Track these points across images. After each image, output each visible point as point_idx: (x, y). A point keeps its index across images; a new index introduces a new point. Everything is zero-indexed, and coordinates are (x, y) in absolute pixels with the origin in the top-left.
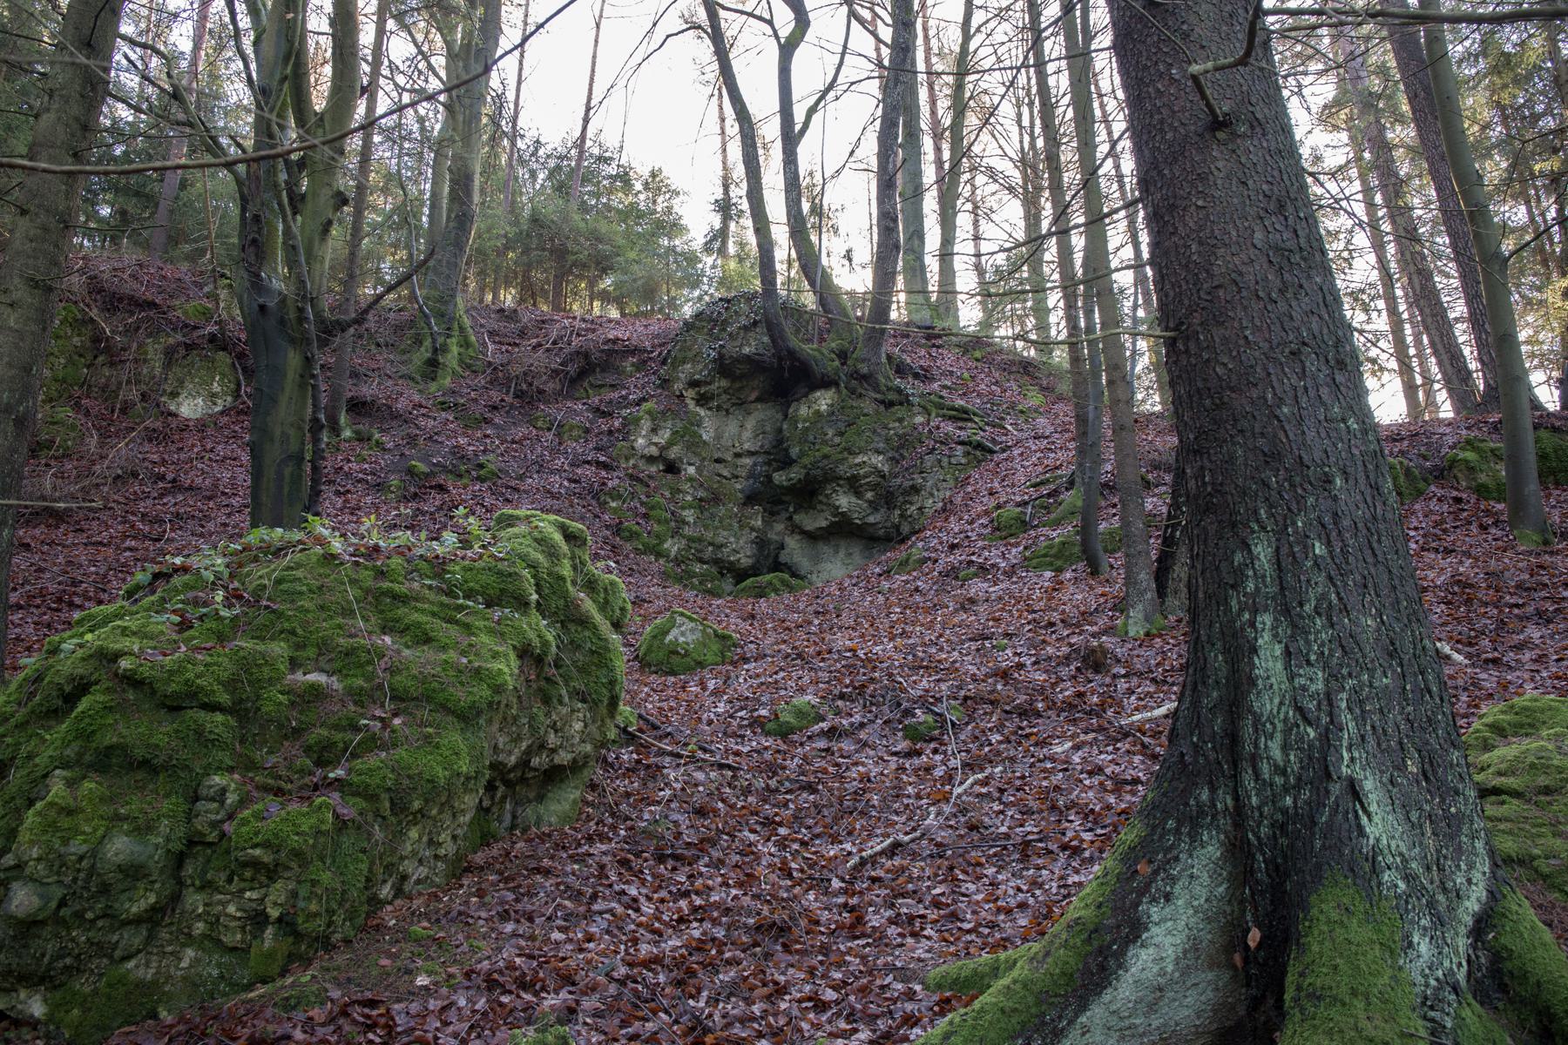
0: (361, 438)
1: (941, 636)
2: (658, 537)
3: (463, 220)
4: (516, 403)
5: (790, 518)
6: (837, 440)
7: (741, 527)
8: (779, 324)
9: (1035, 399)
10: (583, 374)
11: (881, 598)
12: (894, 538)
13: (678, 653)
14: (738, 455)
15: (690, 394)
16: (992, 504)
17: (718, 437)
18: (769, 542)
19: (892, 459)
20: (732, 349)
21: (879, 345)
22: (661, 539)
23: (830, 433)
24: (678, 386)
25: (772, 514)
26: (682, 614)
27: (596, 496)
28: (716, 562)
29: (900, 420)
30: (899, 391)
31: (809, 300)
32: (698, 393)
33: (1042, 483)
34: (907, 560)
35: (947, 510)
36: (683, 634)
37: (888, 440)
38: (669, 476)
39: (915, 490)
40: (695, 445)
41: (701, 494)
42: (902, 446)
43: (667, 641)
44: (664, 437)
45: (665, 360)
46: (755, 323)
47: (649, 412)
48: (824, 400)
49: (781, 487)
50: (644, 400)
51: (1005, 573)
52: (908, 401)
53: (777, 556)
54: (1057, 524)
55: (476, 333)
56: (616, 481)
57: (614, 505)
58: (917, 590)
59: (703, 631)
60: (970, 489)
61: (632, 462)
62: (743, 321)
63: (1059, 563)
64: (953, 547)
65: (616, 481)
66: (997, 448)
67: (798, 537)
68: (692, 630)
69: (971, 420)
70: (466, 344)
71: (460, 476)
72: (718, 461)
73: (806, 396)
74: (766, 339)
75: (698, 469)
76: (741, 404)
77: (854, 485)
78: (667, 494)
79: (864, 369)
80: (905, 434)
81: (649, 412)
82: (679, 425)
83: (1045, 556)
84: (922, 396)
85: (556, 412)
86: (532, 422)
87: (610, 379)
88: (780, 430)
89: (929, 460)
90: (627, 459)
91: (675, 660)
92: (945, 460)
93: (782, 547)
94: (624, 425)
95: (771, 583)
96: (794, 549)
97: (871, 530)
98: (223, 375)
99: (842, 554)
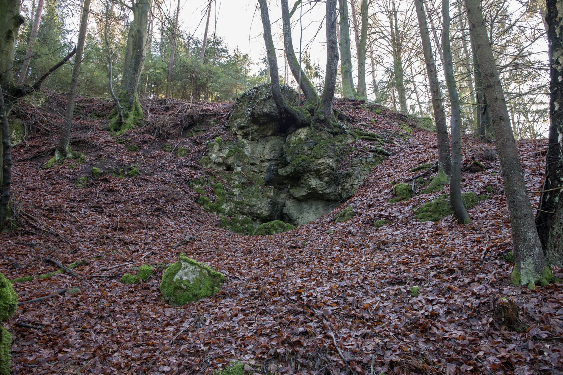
0: (76, 157)
1: (366, 278)
2: (218, 202)
3: (138, 58)
4: (157, 140)
5: (288, 191)
6: (309, 152)
7: (263, 196)
8: (280, 96)
9: (407, 130)
10: (190, 126)
11: (329, 237)
12: (339, 200)
13: (181, 288)
14: (262, 161)
15: (240, 133)
16: (391, 181)
17: (253, 153)
18: (278, 203)
19: (337, 160)
20: (258, 110)
21: (330, 105)
22: (220, 203)
23: (306, 148)
24: (234, 129)
25: (280, 189)
26: (186, 261)
27: (188, 182)
28: (251, 214)
29: (341, 141)
30: (340, 127)
31: (295, 86)
32: (243, 132)
33: (419, 169)
34: (344, 214)
35: (366, 185)
36: (186, 274)
37: (335, 151)
38: (227, 172)
39: (349, 175)
40: (240, 156)
41: (243, 180)
42: (342, 154)
43: (174, 280)
44: (225, 153)
45: (228, 117)
46: (269, 97)
47: (218, 142)
48: (303, 133)
49: (283, 176)
50: (217, 136)
51: (402, 222)
52: (344, 132)
53: (282, 210)
54: (431, 191)
55: (143, 109)
56: (199, 175)
57: (197, 187)
58: (349, 232)
59: (201, 272)
60: (377, 174)
61: (209, 166)
62: (264, 97)
63: (436, 216)
64: (370, 206)
65: (199, 175)
66: (390, 153)
67: (292, 200)
68: (193, 272)
69: (376, 140)
70: (138, 114)
71: (119, 174)
72: (252, 164)
73: (294, 131)
74: (274, 105)
75: (242, 168)
76: (264, 137)
77: (318, 174)
78: (225, 181)
79: (322, 117)
80: (343, 148)
81: (218, 142)
82: (233, 147)
83: (426, 211)
84: (351, 129)
85: (175, 143)
86: (163, 148)
87: (203, 127)
88: (282, 149)
89: (356, 160)
90: (207, 164)
91: (179, 293)
92: (364, 160)
93: (284, 205)
94: (206, 148)
95: (273, 226)
96: (291, 207)
97: (328, 196)
98: (17, 130)
99: (313, 209)
